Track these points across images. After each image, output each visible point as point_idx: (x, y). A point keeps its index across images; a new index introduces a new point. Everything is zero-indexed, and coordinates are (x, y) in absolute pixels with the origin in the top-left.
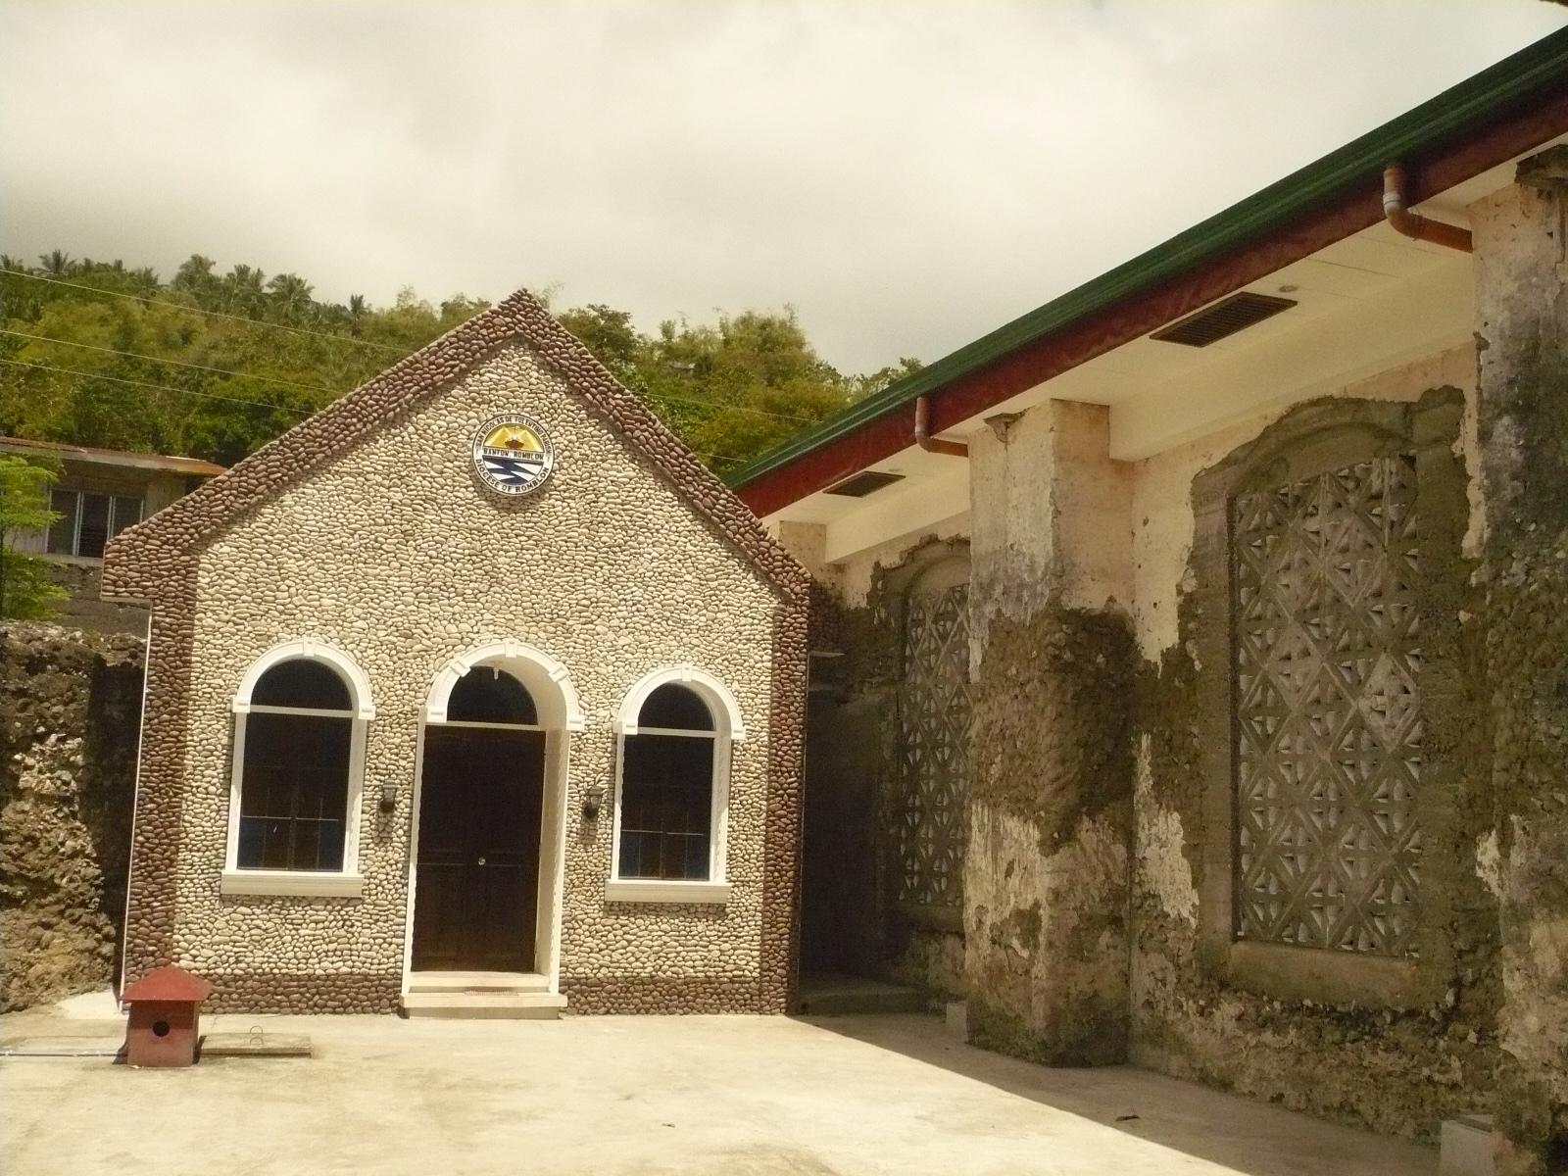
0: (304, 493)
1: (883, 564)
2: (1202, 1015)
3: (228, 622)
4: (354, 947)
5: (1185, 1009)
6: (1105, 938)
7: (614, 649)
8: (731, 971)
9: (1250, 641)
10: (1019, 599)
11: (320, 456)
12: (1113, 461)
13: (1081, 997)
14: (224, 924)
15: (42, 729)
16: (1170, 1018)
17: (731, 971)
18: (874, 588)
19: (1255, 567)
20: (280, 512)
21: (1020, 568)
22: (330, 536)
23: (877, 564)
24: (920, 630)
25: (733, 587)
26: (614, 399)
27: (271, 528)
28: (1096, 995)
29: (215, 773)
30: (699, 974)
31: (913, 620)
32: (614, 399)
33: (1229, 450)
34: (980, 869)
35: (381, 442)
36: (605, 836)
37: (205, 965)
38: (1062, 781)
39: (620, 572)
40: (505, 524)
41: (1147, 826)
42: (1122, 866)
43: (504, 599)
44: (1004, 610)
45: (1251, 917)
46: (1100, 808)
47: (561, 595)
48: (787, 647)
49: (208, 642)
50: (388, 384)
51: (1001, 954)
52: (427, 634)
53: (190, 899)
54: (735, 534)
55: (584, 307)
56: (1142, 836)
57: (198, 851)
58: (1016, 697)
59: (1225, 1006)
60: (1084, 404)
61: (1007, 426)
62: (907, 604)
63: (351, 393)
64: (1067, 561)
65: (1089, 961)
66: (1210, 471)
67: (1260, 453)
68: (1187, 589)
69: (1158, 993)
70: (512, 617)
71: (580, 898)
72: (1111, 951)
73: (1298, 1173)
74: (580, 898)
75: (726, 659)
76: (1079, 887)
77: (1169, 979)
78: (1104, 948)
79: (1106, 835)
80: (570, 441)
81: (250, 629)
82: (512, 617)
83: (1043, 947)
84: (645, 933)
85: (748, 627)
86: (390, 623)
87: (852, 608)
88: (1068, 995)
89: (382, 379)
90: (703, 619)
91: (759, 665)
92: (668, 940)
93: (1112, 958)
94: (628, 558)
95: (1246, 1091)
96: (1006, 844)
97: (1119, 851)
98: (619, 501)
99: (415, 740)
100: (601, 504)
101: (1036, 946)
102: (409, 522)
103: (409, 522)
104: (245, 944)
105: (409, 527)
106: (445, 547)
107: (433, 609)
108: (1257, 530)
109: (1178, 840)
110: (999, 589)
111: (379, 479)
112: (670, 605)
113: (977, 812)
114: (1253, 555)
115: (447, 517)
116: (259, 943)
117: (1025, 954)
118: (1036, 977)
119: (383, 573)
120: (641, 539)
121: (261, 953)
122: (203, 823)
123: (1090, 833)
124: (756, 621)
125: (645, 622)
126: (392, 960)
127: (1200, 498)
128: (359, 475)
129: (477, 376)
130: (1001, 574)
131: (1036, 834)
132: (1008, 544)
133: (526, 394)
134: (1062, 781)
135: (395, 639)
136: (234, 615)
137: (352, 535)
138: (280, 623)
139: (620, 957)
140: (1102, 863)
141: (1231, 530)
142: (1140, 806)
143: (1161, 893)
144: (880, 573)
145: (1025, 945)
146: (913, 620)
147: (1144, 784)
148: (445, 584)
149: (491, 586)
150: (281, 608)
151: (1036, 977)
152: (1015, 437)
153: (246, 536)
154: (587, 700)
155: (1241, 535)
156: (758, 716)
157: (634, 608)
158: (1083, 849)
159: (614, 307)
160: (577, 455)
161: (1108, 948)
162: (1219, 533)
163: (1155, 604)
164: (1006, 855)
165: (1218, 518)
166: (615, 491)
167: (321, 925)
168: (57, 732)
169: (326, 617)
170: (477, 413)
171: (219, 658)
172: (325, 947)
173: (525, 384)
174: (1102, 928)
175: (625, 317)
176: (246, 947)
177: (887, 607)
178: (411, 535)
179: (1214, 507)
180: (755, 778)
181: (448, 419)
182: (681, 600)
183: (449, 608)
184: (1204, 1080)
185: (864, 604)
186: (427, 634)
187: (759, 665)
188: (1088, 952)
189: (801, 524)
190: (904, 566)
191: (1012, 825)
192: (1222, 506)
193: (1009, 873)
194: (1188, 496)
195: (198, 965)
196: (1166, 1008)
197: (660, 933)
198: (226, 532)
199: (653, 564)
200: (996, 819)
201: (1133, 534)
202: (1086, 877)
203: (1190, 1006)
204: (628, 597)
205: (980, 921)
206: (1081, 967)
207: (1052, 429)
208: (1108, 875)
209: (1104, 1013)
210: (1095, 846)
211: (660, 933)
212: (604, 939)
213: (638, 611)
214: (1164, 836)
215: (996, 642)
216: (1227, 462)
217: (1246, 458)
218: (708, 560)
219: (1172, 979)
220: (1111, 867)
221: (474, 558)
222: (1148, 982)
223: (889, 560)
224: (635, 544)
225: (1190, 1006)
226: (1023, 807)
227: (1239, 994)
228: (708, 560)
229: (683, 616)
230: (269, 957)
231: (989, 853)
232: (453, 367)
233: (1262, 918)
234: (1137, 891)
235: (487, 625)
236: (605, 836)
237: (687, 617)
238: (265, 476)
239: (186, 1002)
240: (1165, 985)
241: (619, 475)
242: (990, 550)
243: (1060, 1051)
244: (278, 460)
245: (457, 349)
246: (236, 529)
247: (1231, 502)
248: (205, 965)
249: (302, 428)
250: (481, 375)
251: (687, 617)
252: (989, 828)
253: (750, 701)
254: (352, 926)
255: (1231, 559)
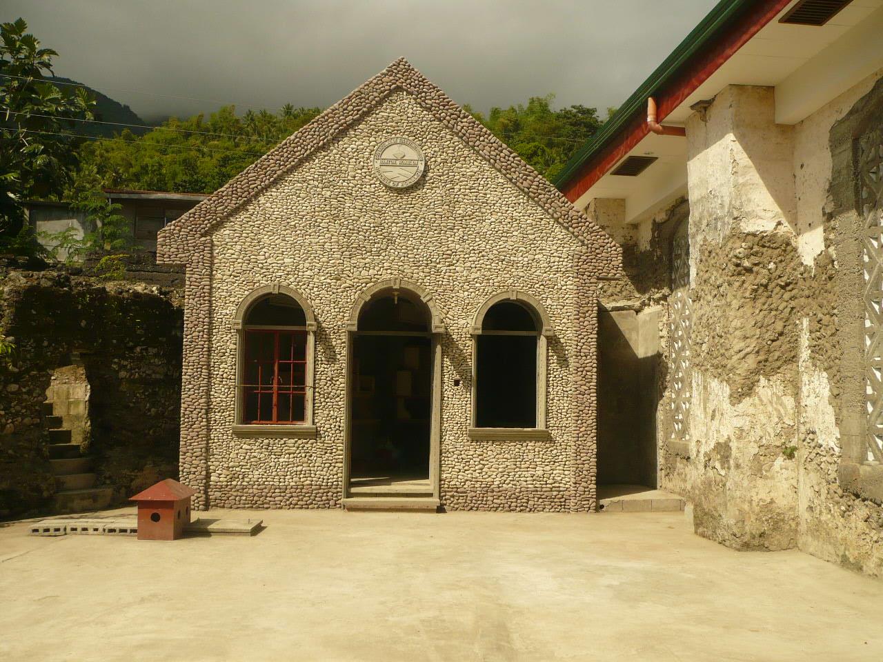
0: (271, 195)
1: (657, 220)
2: (843, 517)
3: (230, 276)
4: (312, 469)
5: (832, 512)
6: (780, 461)
7: (467, 281)
8: (551, 484)
9: (870, 242)
10: (716, 228)
11: (279, 172)
12: (778, 125)
13: (761, 503)
14: (235, 456)
15: (131, 344)
16: (823, 518)
17: (551, 484)
18: (653, 237)
19: (873, 187)
20: (258, 208)
21: (715, 207)
22: (289, 220)
23: (654, 221)
24: (679, 261)
25: (545, 238)
26: (462, 122)
27: (253, 218)
28: (772, 502)
29: (226, 366)
30: (530, 486)
31: (676, 255)
32: (462, 122)
33: (854, 102)
34: (697, 416)
35: (317, 161)
36: (466, 399)
37: (225, 479)
38: (744, 352)
39: (470, 232)
40: (395, 206)
41: (807, 383)
42: (792, 411)
43: (396, 253)
44: (707, 237)
45: (874, 446)
46: (775, 371)
47: (434, 248)
48: (583, 275)
49: (219, 288)
50: (319, 124)
51: (711, 473)
52: (349, 276)
53: (216, 441)
54: (545, 204)
55: (569, 108)
56: (805, 389)
57: (219, 412)
58: (715, 296)
59: (857, 511)
60: (754, 86)
61: (705, 109)
62: (672, 244)
63: (296, 132)
64: (744, 198)
65: (766, 478)
66: (840, 122)
67: (874, 101)
68: (828, 210)
69: (816, 501)
70: (401, 264)
71: (451, 438)
72: (784, 470)
73: (725, 660)
74: (451, 438)
75: (542, 285)
76: (758, 427)
77: (822, 490)
78: (778, 469)
79: (779, 388)
80: (435, 152)
81: (243, 279)
82: (401, 264)
83: (732, 468)
84: (494, 460)
85: (556, 263)
86: (327, 271)
87: (643, 251)
88: (751, 502)
89: (315, 122)
90: (526, 259)
91: (564, 288)
92: (509, 464)
93: (784, 476)
94: (475, 223)
95: (871, 573)
96: (711, 397)
97: (789, 401)
98: (467, 187)
99: (344, 342)
100: (456, 191)
101: (729, 468)
102: (336, 208)
103: (336, 208)
104: (248, 467)
105: (336, 212)
106: (358, 223)
107: (352, 261)
108: (872, 160)
109: (826, 392)
110: (705, 222)
111: (316, 183)
112: (504, 252)
113: (695, 376)
114: (871, 179)
115: (358, 204)
116: (257, 467)
117: (723, 473)
118: (729, 489)
119: (321, 241)
120: (483, 210)
121: (257, 473)
122: (221, 396)
123: (765, 389)
124: (561, 259)
125: (487, 263)
126: (335, 476)
127: (835, 143)
128: (304, 181)
129: (374, 115)
130: (705, 213)
131: (727, 390)
132: (709, 191)
133: (405, 124)
134: (744, 352)
135: (330, 281)
136: (234, 271)
137: (302, 219)
138: (260, 274)
139: (478, 475)
140: (776, 409)
141: (856, 162)
142: (803, 369)
143: (817, 430)
144: (657, 226)
145: (723, 468)
146: (676, 255)
147: (805, 354)
148: (359, 245)
149: (388, 246)
150: (260, 265)
151: (729, 489)
152: (710, 116)
153: (238, 223)
154: (452, 314)
155: (863, 167)
156: (565, 320)
157: (480, 255)
158: (761, 400)
159: (588, 105)
160: (439, 160)
161: (781, 469)
162: (848, 166)
163: (810, 224)
164: (711, 407)
165: (847, 156)
166: (465, 181)
167: (292, 456)
168: (141, 346)
169: (288, 270)
170: (375, 138)
171: (225, 298)
172: (295, 469)
173: (405, 117)
174: (776, 455)
175: (594, 110)
176: (249, 469)
177: (660, 247)
178: (337, 217)
179: (844, 147)
180: (564, 361)
181: (357, 143)
182: (511, 248)
183: (362, 260)
184: (845, 562)
185: (648, 248)
186: (349, 276)
187: (564, 288)
188: (766, 471)
189: (608, 199)
190: (669, 220)
191: (714, 384)
192: (849, 146)
193: (713, 418)
194: (828, 142)
195: (221, 479)
196: (821, 511)
197: (504, 460)
198: (227, 222)
199: (492, 226)
200: (705, 381)
201: (795, 176)
202: (763, 418)
203: (836, 511)
204: (476, 248)
205: (698, 451)
206: (760, 482)
207: (731, 106)
208: (780, 418)
209: (779, 514)
210: (770, 398)
211: (504, 460)
212: (467, 463)
213: (483, 256)
214: (817, 386)
215: (704, 259)
216: (851, 113)
217: (863, 107)
218: (528, 222)
219: (824, 491)
220: (782, 411)
221: (377, 228)
222: (810, 493)
223: (661, 217)
224: (480, 214)
225: (836, 511)
226: (721, 370)
227: (866, 502)
228: (528, 222)
229: (512, 258)
230: (263, 475)
231: (702, 404)
232: (358, 110)
233: (881, 447)
234: (803, 429)
235: (387, 270)
236: (466, 399)
237: (516, 259)
238: (247, 187)
239: (169, 501)
240: (820, 495)
241: (468, 170)
242: (699, 197)
243: (746, 540)
244: (255, 176)
245: (361, 99)
246: (232, 219)
247: (856, 141)
248: (225, 479)
249: (268, 156)
250: (376, 114)
251: (516, 259)
252: (701, 387)
253: (559, 311)
254: (311, 456)
255: (856, 184)
